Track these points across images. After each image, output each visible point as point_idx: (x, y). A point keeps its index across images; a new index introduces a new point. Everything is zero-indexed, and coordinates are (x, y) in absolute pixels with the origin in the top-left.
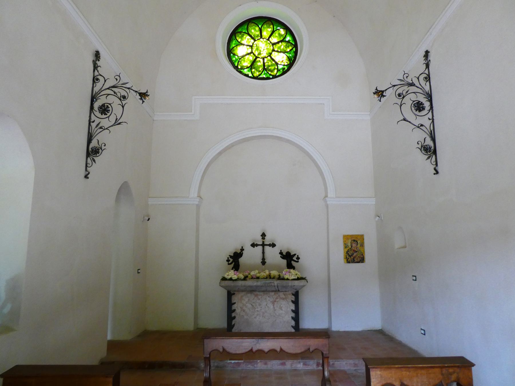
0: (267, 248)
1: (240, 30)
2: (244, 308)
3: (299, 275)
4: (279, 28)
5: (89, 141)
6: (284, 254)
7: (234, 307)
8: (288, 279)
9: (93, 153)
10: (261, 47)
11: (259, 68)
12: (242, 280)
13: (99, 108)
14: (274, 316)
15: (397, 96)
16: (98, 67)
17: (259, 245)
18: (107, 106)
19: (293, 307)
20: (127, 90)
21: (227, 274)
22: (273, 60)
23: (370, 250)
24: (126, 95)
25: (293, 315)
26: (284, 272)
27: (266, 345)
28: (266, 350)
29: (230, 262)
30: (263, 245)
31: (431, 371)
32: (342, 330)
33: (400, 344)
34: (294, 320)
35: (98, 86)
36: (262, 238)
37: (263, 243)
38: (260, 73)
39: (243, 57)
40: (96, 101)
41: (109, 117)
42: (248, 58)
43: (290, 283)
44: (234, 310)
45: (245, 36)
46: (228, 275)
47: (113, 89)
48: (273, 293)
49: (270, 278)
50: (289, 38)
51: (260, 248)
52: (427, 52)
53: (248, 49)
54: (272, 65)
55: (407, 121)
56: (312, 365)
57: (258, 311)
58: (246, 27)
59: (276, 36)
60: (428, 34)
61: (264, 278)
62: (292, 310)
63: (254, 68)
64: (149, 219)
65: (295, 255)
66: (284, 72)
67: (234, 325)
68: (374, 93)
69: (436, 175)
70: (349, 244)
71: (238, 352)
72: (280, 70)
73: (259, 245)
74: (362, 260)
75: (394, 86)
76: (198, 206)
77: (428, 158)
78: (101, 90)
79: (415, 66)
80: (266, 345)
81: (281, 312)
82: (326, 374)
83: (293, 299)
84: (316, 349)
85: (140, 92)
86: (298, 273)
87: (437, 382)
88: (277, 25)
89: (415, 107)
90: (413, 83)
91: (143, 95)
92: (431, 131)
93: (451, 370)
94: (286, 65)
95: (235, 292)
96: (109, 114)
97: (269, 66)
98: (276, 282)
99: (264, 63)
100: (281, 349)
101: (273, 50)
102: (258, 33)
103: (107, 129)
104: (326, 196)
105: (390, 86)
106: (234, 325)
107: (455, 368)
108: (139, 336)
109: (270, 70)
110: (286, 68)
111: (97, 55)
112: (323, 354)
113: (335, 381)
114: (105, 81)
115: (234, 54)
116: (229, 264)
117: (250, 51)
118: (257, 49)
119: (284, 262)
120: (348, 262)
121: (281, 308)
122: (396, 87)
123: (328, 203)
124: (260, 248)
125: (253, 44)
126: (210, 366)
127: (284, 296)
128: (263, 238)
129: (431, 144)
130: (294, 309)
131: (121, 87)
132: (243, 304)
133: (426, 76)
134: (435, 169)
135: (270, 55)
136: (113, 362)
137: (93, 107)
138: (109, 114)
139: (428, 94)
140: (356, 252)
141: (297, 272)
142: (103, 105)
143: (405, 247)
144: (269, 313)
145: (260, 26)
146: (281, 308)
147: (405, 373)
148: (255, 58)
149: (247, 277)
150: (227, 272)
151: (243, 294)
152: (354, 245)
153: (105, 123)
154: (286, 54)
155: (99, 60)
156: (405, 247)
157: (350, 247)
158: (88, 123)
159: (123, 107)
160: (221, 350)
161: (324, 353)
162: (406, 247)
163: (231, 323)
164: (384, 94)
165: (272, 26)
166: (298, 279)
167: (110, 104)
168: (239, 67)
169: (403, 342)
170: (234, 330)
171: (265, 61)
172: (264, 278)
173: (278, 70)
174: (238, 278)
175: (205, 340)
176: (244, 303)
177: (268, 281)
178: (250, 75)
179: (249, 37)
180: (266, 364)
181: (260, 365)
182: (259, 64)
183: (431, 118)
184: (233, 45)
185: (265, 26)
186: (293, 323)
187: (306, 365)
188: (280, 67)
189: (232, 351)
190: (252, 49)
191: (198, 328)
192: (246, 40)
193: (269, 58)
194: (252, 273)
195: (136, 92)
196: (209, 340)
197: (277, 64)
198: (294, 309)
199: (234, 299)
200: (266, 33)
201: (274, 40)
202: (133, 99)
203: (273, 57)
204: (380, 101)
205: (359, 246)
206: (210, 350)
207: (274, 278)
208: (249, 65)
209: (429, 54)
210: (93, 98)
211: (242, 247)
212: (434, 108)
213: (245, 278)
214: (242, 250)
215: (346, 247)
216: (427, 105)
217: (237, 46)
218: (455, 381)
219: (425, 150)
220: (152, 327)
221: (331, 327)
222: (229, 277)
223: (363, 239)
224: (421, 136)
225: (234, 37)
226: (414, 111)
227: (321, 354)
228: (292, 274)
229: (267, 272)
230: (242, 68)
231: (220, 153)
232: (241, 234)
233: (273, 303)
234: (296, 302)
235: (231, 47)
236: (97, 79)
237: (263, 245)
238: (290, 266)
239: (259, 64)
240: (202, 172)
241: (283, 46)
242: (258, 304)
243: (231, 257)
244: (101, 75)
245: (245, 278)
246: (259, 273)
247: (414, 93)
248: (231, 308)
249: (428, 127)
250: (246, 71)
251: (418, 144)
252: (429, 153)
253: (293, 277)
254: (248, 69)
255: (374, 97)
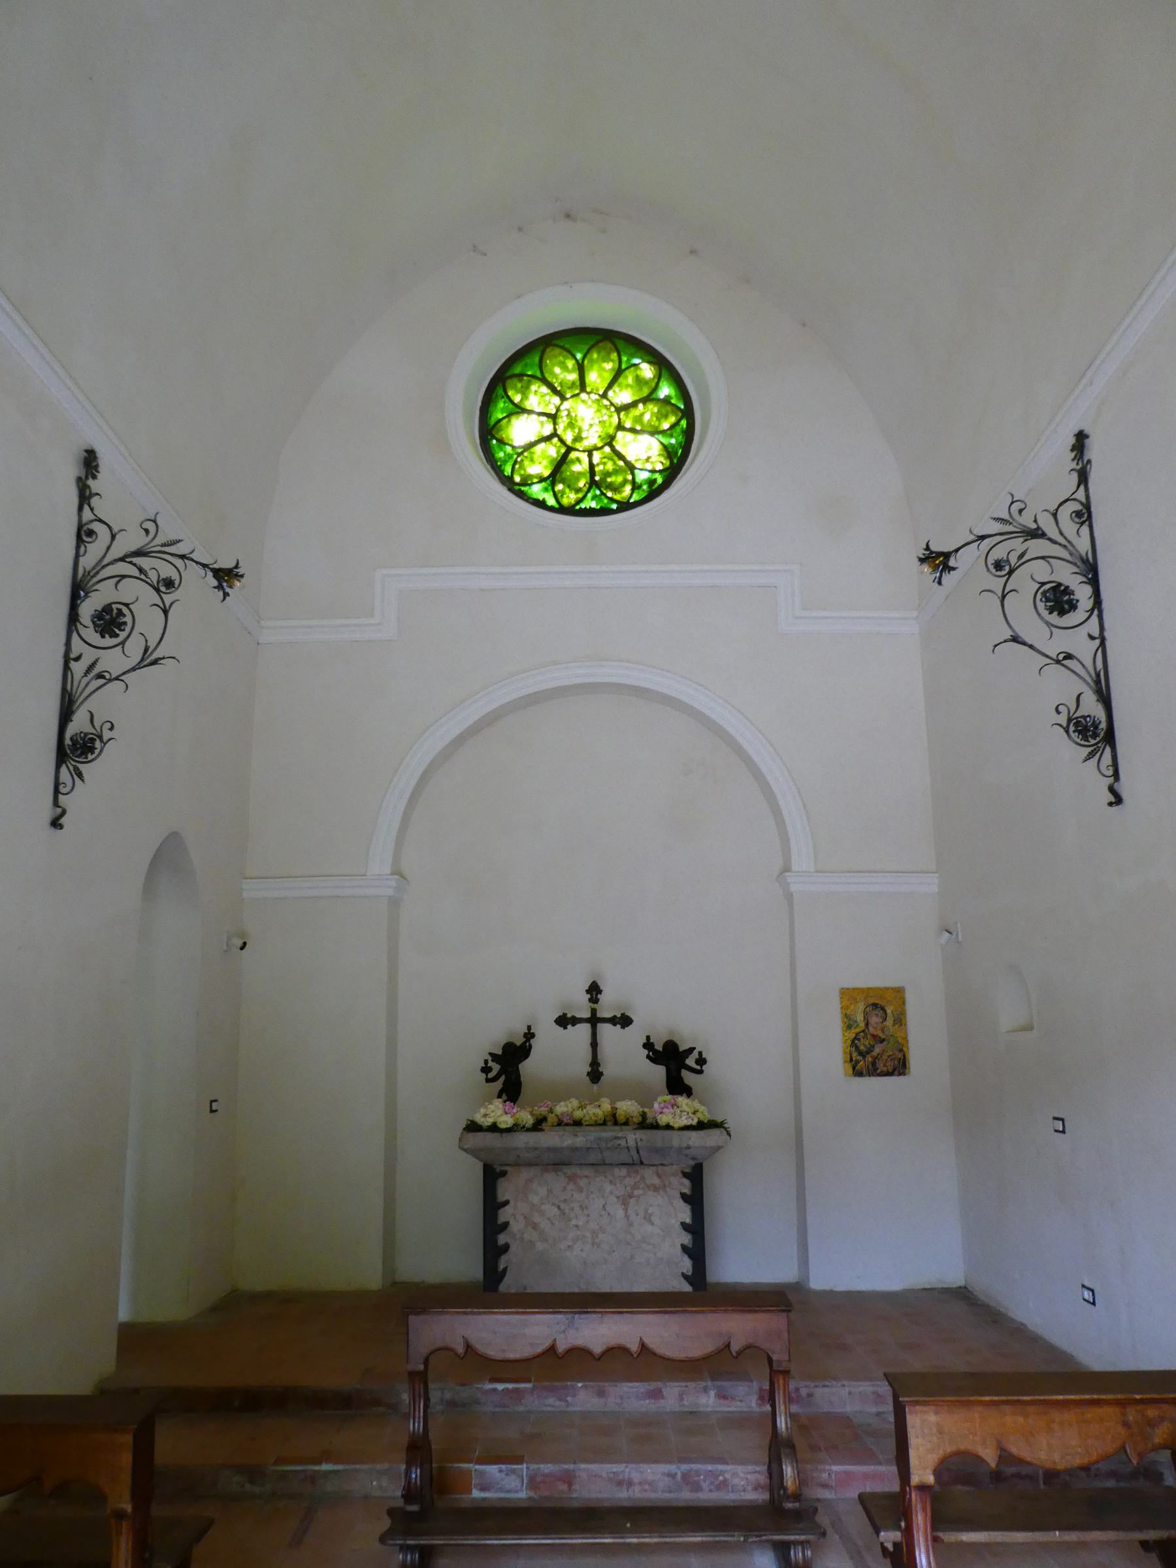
0: (605, 1029)
1: (517, 370)
2: (537, 1219)
3: (705, 1115)
4: (636, 361)
5: (66, 715)
6: (659, 1047)
7: (504, 1215)
8: (668, 1127)
9: (75, 751)
10: (586, 417)
11: (578, 480)
12: (528, 1130)
13: (93, 617)
14: (628, 1244)
15: (991, 568)
16: (92, 495)
17: (581, 1021)
18: (119, 611)
19: (685, 1214)
20: (179, 562)
21: (483, 1111)
22: (621, 457)
23: (925, 1035)
24: (175, 576)
25: (686, 1239)
26: (656, 1105)
27: (598, 1332)
28: (597, 1349)
29: (490, 1075)
30: (594, 1020)
31: (1092, 1413)
32: (841, 1287)
33: (1020, 1332)
34: (690, 1257)
35: (93, 552)
36: (590, 1000)
37: (595, 1014)
38: (580, 495)
39: (530, 446)
40: (86, 596)
41: (123, 643)
42: (544, 451)
43: (676, 1139)
44: (506, 1225)
45: (533, 388)
46: (485, 1115)
47: (135, 560)
48: (624, 1171)
49: (616, 1123)
50: (666, 390)
51: (584, 1030)
52: (1080, 441)
53: (542, 423)
54: (616, 472)
55: (1024, 643)
56: (746, 1398)
57: (577, 1226)
58: (537, 359)
59: (628, 386)
60: (1084, 381)
61: (596, 1124)
62: (683, 1224)
63: (563, 481)
64: (245, 944)
65: (692, 1050)
66: (655, 492)
67: (505, 1270)
68: (922, 561)
69: (1115, 808)
70: (860, 1017)
71: (511, 1356)
72: (640, 487)
73: (581, 1021)
74: (900, 1067)
75: (982, 538)
76: (394, 903)
77: (1091, 755)
78: (100, 565)
79: (1046, 479)
80: (598, 1332)
81: (649, 1228)
82: (782, 1423)
83: (687, 1191)
84: (749, 1347)
85: (216, 566)
86: (702, 1108)
87: (1110, 1447)
88: (633, 350)
89: (1048, 600)
90: (1038, 528)
91: (225, 577)
92: (1098, 675)
93: (1152, 1412)
94: (660, 471)
95: (508, 1168)
96: (123, 635)
97: (608, 474)
98: (632, 1137)
99: (592, 466)
100: (643, 1346)
101: (620, 427)
102: (574, 376)
103: (117, 679)
104: (787, 869)
105: (972, 538)
106: (505, 1270)
107: (1165, 1407)
108: (214, 1309)
109: (611, 487)
110: (660, 480)
111: (90, 462)
112: (770, 1360)
113: (814, 1448)
114: (113, 537)
115: (501, 442)
116: (488, 1080)
117: (548, 429)
118: (571, 425)
119: (660, 1071)
120: (858, 1073)
121: (648, 1218)
122: (987, 543)
123: (793, 888)
124: (584, 1030)
125: (558, 409)
126: (427, 1399)
127: (656, 1181)
128: (594, 1000)
129: (1099, 713)
130: (688, 1221)
131: (160, 554)
132: (532, 1204)
133: (1078, 507)
134: (1111, 789)
135: (610, 441)
136: (136, 1391)
137: (77, 614)
138: (123, 635)
139: (1085, 561)
140: (882, 1041)
141: (697, 1105)
142: (107, 609)
143: (1029, 1028)
144: (615, 1232)
145: (579, 356)
146: (648, 1218)
147: (1012, 1420)
148: (563, 450)
149: (545, 1119)
150: (482, 1105)
151: (533, 1171)
152: (874, 1020)
153: (113, 661)
154: (660, 437)
155: (94, 477)
156: (1029, 1028)
157: (862, 1025)
158: (61, 661)
159: (166, 612)
160: (461, 1350)
161: (775, 1358)
162: (1032, 1029)
163: (496, 1267)
164: (952, 563)
165: (614, 356)
166: (701, 1126)
167: (127, 605)
168: (517, 479)
169: (1031, 1327)
170: (502, 1288)
171: (596, 460)
172: (596, 1124)
173: (636, 487)
174: (516, 1125)
175: (412, 1319)
176: (535, 1199)
177: (608, 1133)
178: (551, 502)
179: (544, 389)
180: (601, 1393)
181: (583, 1398)
182: (576, 468)
183: (1096, 633)
184: (499, 411)
185: (595, 356)
186: (687, 1265)
187: (725, 1398)
188: (641, 476)
189: (493, 1352)
190: (555, 424)
191: (395, 1283)
192: (538, 398)
193: (607, 449)
194: (561, 1108)
195: (205, 566)
196: (421, 1317)
197: (631, 468)
198: (688, 1221)
199: (505, 1190)
200: (597, 377)
201: (623, 395)
202: (196, 586)
203: (618, 448)
204: (940, 583)
205: (889, 1022)
206: (425, 1351)
207: (626, 1123)
208: (546, 473)
209: (1087, 441)
210: (78, 589)
211: (529, 1027)
212: (1105, 605)
213: (539, 1124)
214: (529, 1035)
215: (849, 1027)
216: (1083, 594)
217: (509, 416)
218: (1164, 1447)
219: (1080, 732)
220: (255, 1281)
221: (807, 1277)
222: (488, 1121)
223: (904, 1003)
224: (1067, 689)
225: (500, 391)
226: (1045, 613)
227: (766, 1363)
228: (679, 1112)
229: (606, 1106)
230: (526, 482)
231: (460, 741)
232: (525, 988)
233: (625, 1201)
234: (695, 1199)
235: (492, 421)
236: (91, 533)
237: (594, 1020)
238: (677, 1086)
239: (576, 468)
240: (407, 796)
241: (648, 412)
242: (576, 1206)
243: (494, 1057)
244: (100, 521)
245: (539, 1124)
246: (581, 1107)
247: (1043, 558)
248: (495, 1216)
249: (1089, 663)
250: (537, 491)
251: (1058, 712)
252: (1093, 742)
253: (685, 1121)
254: (543, 484)
255: (922, 572)
